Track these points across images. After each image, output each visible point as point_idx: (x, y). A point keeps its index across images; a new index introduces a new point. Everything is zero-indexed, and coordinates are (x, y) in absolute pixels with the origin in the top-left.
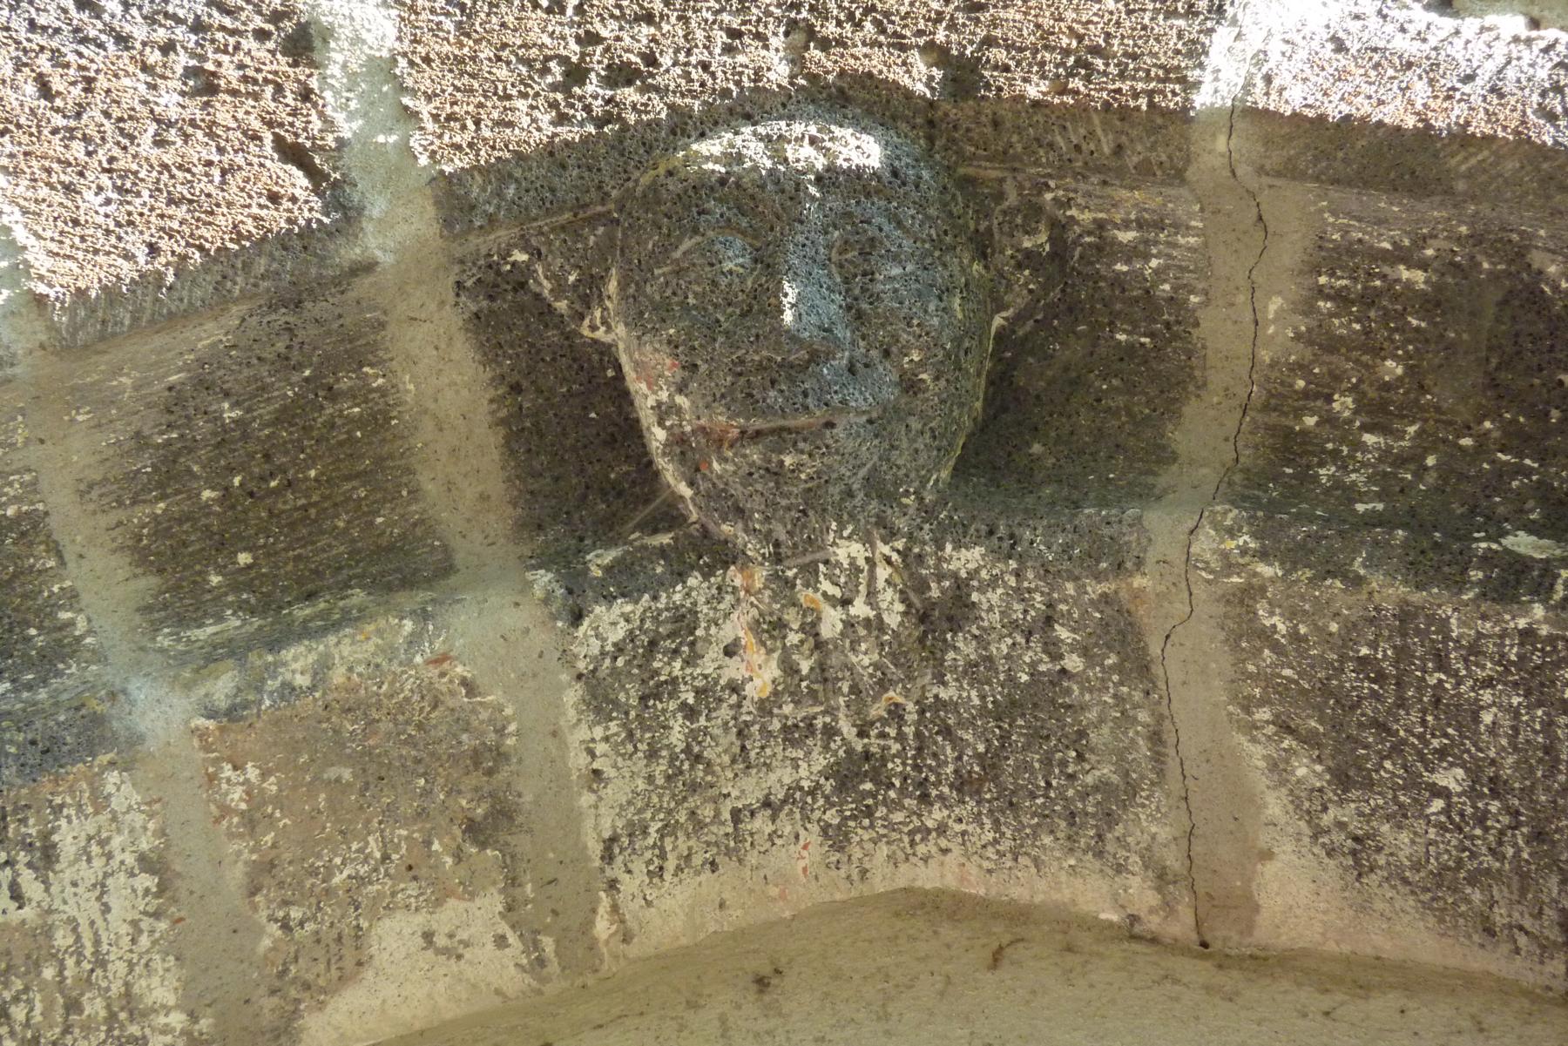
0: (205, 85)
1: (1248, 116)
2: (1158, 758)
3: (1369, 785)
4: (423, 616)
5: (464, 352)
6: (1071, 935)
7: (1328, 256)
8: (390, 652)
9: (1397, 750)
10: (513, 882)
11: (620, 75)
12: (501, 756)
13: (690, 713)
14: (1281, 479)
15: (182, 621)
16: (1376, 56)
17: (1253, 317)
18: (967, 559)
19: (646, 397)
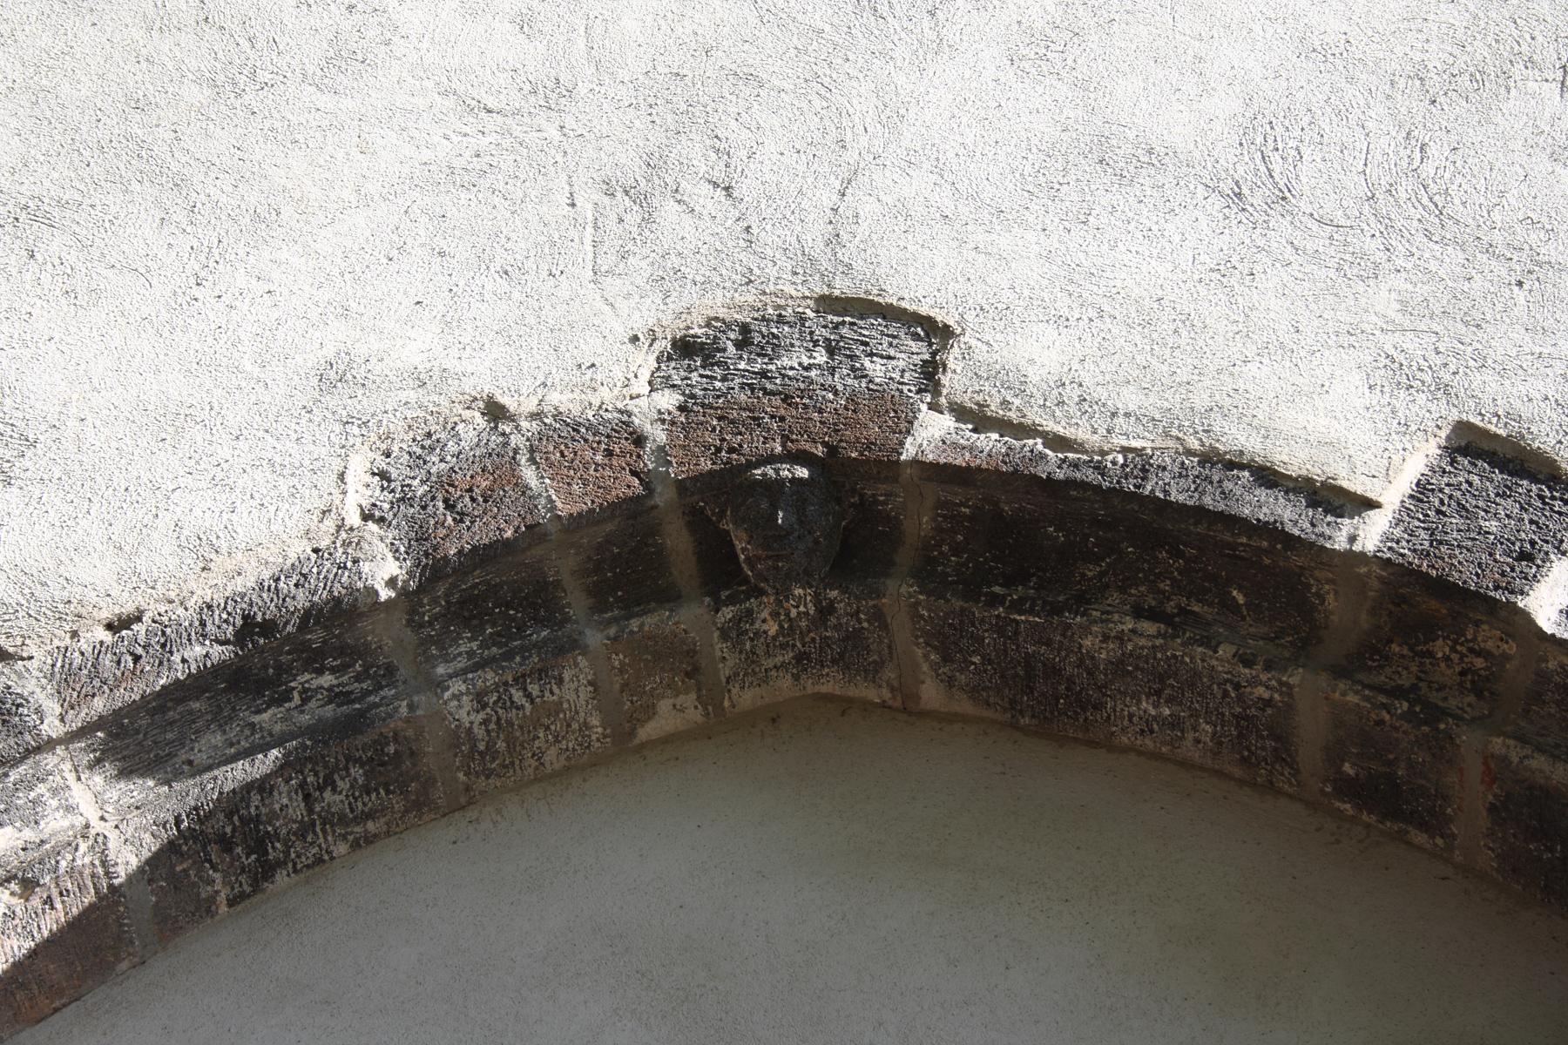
0: (609, 453)
1: (915, 462)
2: (890, 653)
3: (952, 661)
4: (671, 610)
5: (685, 532)
6: (866, 707)
7: (940, 504)
8: (662, 621)
9: (960, 651)
10: (700, 689)
11: (731, 450)
12: (695, 652)
13: (752, 640)
14: (927, 573)
15: (602, 611)
16: (955, 445)
17: (920, 522)
18: (834, 594)
19: (739, 546)
